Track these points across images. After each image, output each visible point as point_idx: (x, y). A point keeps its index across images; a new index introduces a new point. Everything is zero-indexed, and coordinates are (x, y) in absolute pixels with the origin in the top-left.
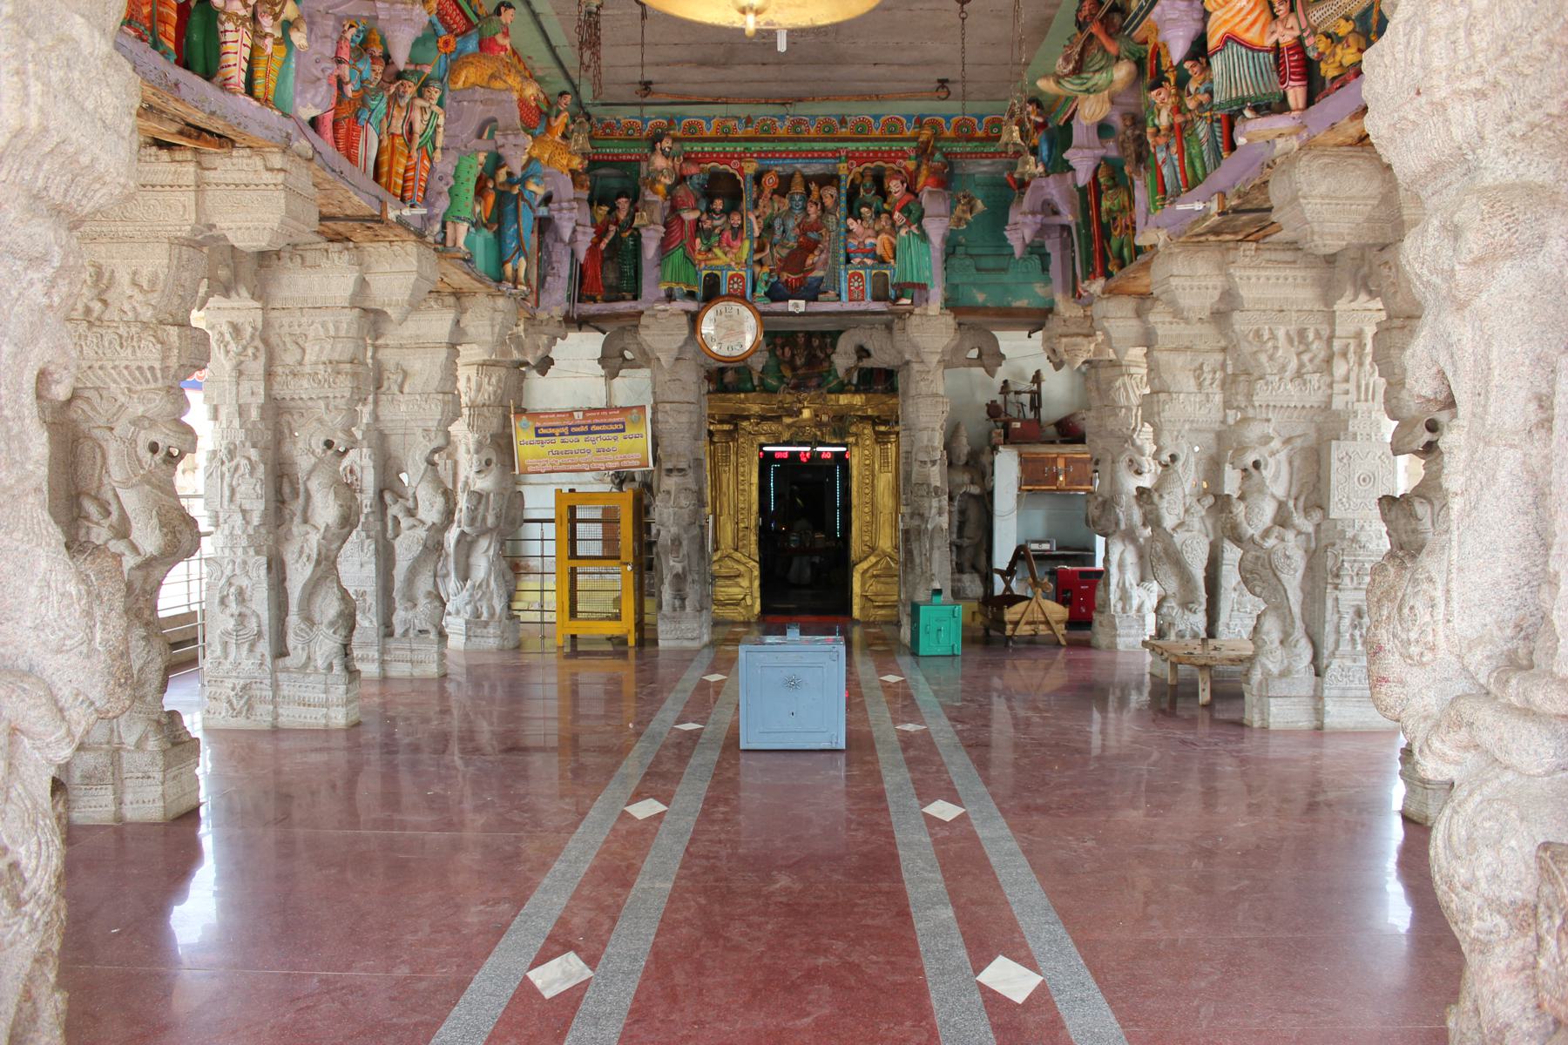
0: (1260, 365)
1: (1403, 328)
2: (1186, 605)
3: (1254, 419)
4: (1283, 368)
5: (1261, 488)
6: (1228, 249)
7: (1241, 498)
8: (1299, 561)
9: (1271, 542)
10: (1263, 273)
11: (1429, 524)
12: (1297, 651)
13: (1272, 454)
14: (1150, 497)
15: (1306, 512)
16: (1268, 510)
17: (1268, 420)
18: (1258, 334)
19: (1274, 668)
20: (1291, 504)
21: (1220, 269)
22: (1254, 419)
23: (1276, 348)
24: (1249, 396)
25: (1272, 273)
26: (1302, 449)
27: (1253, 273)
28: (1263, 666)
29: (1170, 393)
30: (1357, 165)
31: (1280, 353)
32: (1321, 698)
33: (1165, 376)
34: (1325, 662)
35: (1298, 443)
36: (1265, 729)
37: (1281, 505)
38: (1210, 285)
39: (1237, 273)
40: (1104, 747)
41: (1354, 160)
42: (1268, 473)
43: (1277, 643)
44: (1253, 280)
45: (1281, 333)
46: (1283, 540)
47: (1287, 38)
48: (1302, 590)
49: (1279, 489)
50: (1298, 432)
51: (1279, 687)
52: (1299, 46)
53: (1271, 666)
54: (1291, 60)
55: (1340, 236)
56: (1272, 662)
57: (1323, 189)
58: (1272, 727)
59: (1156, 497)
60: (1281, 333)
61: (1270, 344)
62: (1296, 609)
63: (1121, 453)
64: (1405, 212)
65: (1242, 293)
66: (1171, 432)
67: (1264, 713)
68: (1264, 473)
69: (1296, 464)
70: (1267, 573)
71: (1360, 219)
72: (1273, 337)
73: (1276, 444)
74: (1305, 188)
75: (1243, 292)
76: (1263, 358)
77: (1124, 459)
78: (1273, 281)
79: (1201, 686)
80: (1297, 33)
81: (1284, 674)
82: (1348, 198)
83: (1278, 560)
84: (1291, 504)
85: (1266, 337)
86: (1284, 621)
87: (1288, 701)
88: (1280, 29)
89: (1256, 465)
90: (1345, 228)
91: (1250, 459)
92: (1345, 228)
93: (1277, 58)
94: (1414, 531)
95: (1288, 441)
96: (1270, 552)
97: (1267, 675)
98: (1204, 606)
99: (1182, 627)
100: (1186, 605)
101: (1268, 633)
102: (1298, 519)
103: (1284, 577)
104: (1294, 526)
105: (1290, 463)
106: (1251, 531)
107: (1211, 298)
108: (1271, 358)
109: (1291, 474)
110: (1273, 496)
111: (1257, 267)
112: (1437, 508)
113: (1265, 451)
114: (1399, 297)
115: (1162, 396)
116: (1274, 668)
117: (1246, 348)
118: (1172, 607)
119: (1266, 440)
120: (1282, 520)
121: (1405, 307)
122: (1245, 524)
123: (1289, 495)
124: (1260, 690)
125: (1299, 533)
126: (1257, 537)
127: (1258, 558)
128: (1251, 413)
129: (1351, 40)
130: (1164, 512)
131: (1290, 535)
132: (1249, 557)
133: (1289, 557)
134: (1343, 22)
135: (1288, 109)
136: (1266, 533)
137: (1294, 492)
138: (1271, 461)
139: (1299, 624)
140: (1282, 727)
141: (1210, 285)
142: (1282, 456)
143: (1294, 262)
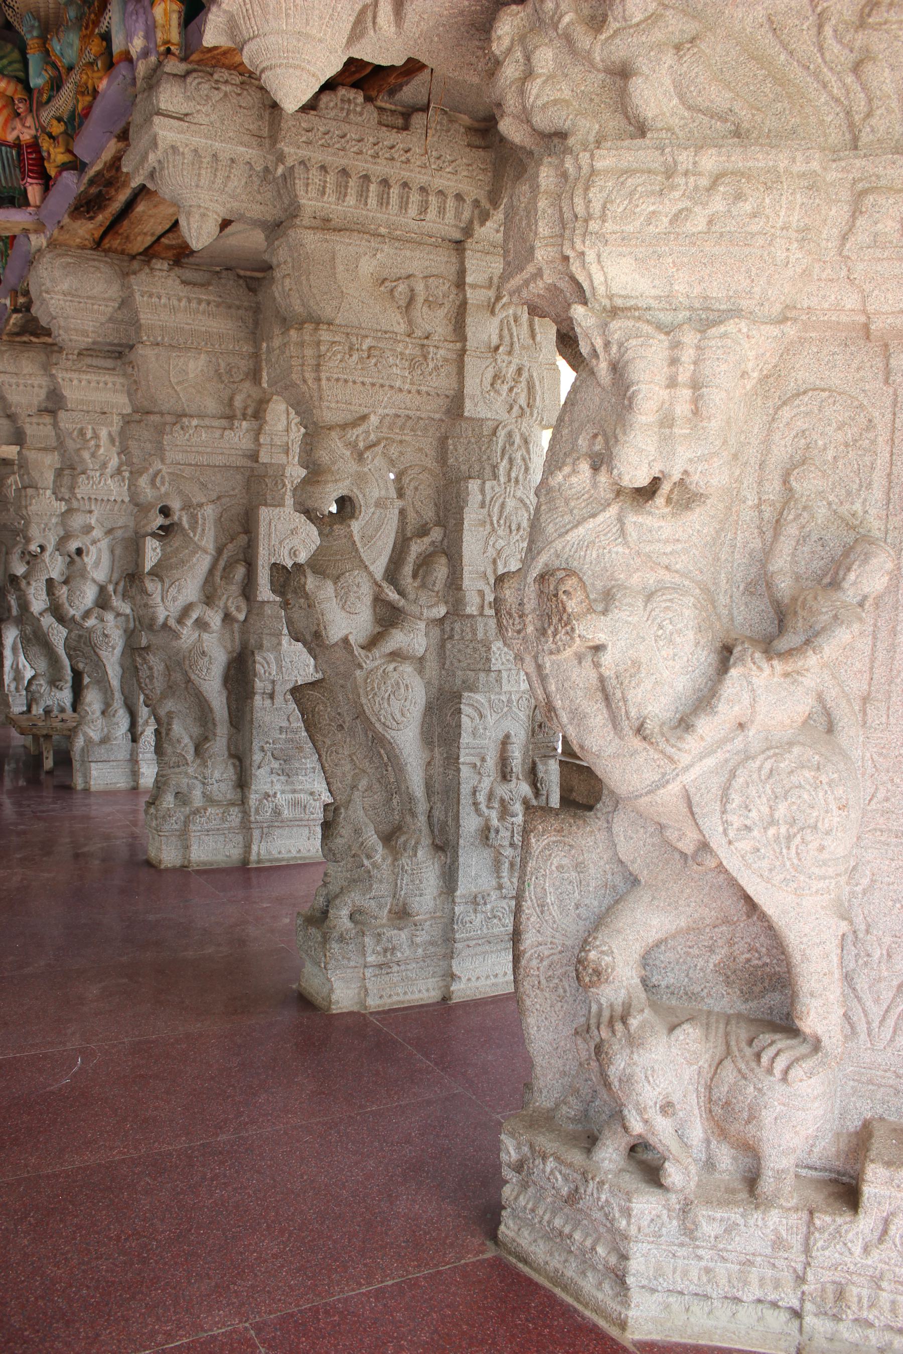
0: (82, 461)
1: (140, 422)
2: (54, 682)
3: (78, 510)
4: (104, 465)
5: (83, 574)
6: (52, 352)
7: (66, 582)
8: (117, 639)
9: (91, 622)
10: (84, 377)
11: (159, 599)
12: (115, 720)
13: (94, 542)
14: (18, 584)
15: (125, 596)
16: (90, 594)
17: (90, 512)
18: (82, 433)
19: (95, 736)
20: (111, 588)
21: (45, 370)
22: (78, 510)
23: (98, 446)
24: (72, 488)
25: (93, 377)
26: (123, 539)
27: (75, 375)
28: (85, 734)
29: (37, 488)
30: (98, 268)
31: (102, 451)
32: (137, 762)
33: (33, 473)
34: (140, 729)
35: (119, 533)
36: (87, 791)
37: (102, 589)
38: (36, 383)
39: (60, 375)
40: (259, 854)
41: (96, 263)
42: (89, 560)
43: (98, 713)
44: (75, 382)
45: (103, 433)
46: (102, 620)
47: (26, 136)
48: (122, 666)
49: (100, 574)
50: (119, 524)
51: (100, 752)
52: (35, 146)
53: (92, 734)
54: (29, 157)
55: (85, 333)
56: (93, 731)
57: (65, 286)
58: (93, 789)
59: (23, 583)
60: (103, 433)
61: (93, 443)
62: (115, 683)
63: (14, 546)
64: (142, 316)
65: (65, 393)
66: (38, 524)
67: (86, 776)
68: (86, 559)
69: (118, 552)
70: (87, 649)
71: (103, 319)
72: (96, 436)
73: (97, 533)
74: (49, 284)
75: (66, 393)
76: (86, 455)
77: (17, 550)
78: (93, 384)
79: (45, 754)
80: (33, 132)
81: (105, 740)
82: (88, 298)
83: (97, 638)
84: (111, 588)
85: (89, 436)
86: (105, 693)
87: (107, 765)
88: (19, 126)
89: (79, 552)
90: (89, 326)
91: (73, 546)
92: (89, 326)
93: (19, 154)
94: (146, 605)
95: (109, 532)
96: (90, 631)
97: (89, 741)
98: (69, 684)
99: (50, 703)
100: (54, 682)
101: (90, 705)
102: (116, 602)
103: (103, 654)
104: (112, 608)
105: (112, 551)
106: (72, 612)
107: (38, 396)
108: (93, 455)
109: (113, 561)
110: (94, 581)
111: (79, 371)
112: (166, 585)
113: (87, 539)
114: (140, 394)
115: (30, 491)
116: (95, 736)
117: (70, 445)
118: (42, 685)
119: (88, 529)
120: (102, 603)
121: (146, 403)
122: (67, 605)
123: (110, 581)
124: (82, 756)
125: (118, 615)
126: (78, 618)
127: (80, 636)
128: (75, 504)
129: (60, 139)
130: (31, 598)
131: (109, 617)
132: (73, 635)
133: (106, 636)
134: (55, 122)
135: (27, 204)
136: (87, 614)
137: (115, 576)
138: (93, 549)
139: (118, 695)
140: (101, 788)
141: (36, 383)
142: (104, 544)
143: (114, 369)
